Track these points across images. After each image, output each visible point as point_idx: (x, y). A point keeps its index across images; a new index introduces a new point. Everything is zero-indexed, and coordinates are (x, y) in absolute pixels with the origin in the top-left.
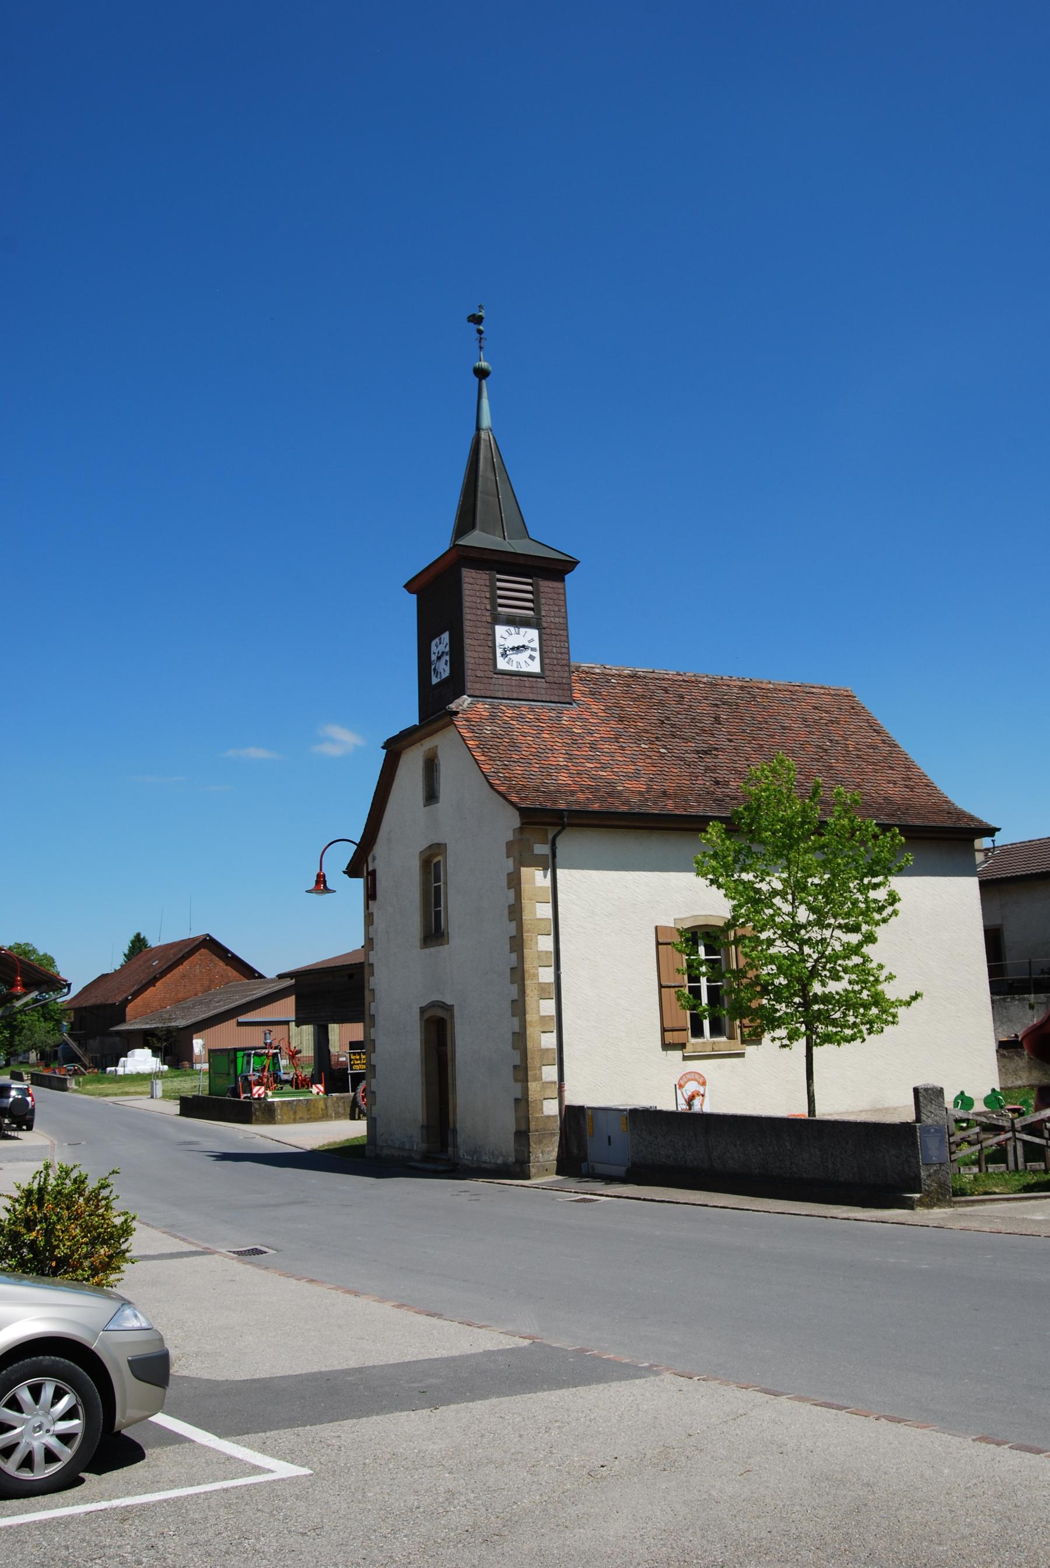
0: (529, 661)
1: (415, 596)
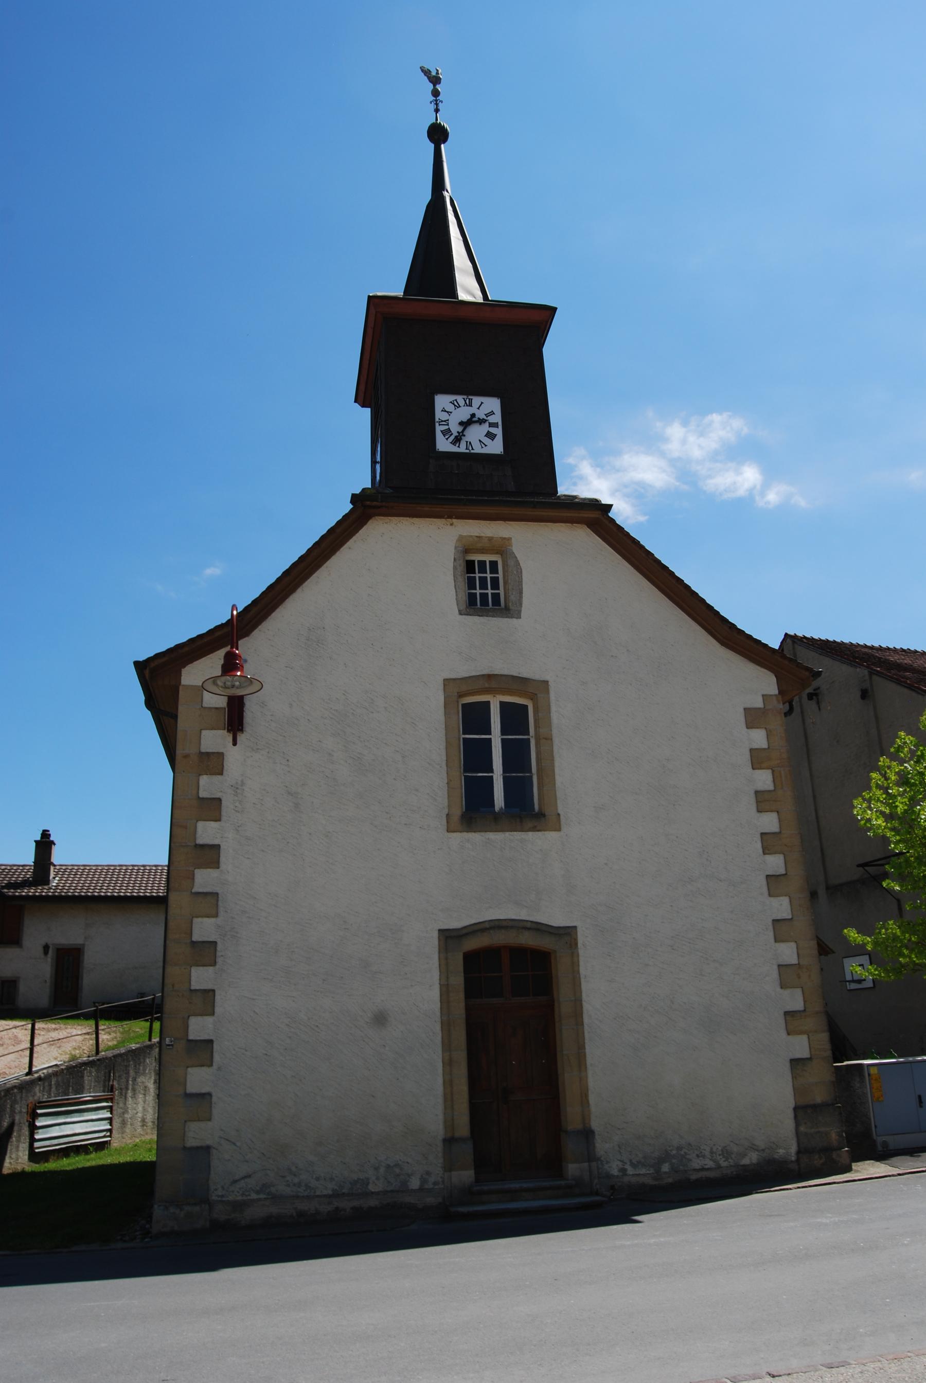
0: (487, 441)
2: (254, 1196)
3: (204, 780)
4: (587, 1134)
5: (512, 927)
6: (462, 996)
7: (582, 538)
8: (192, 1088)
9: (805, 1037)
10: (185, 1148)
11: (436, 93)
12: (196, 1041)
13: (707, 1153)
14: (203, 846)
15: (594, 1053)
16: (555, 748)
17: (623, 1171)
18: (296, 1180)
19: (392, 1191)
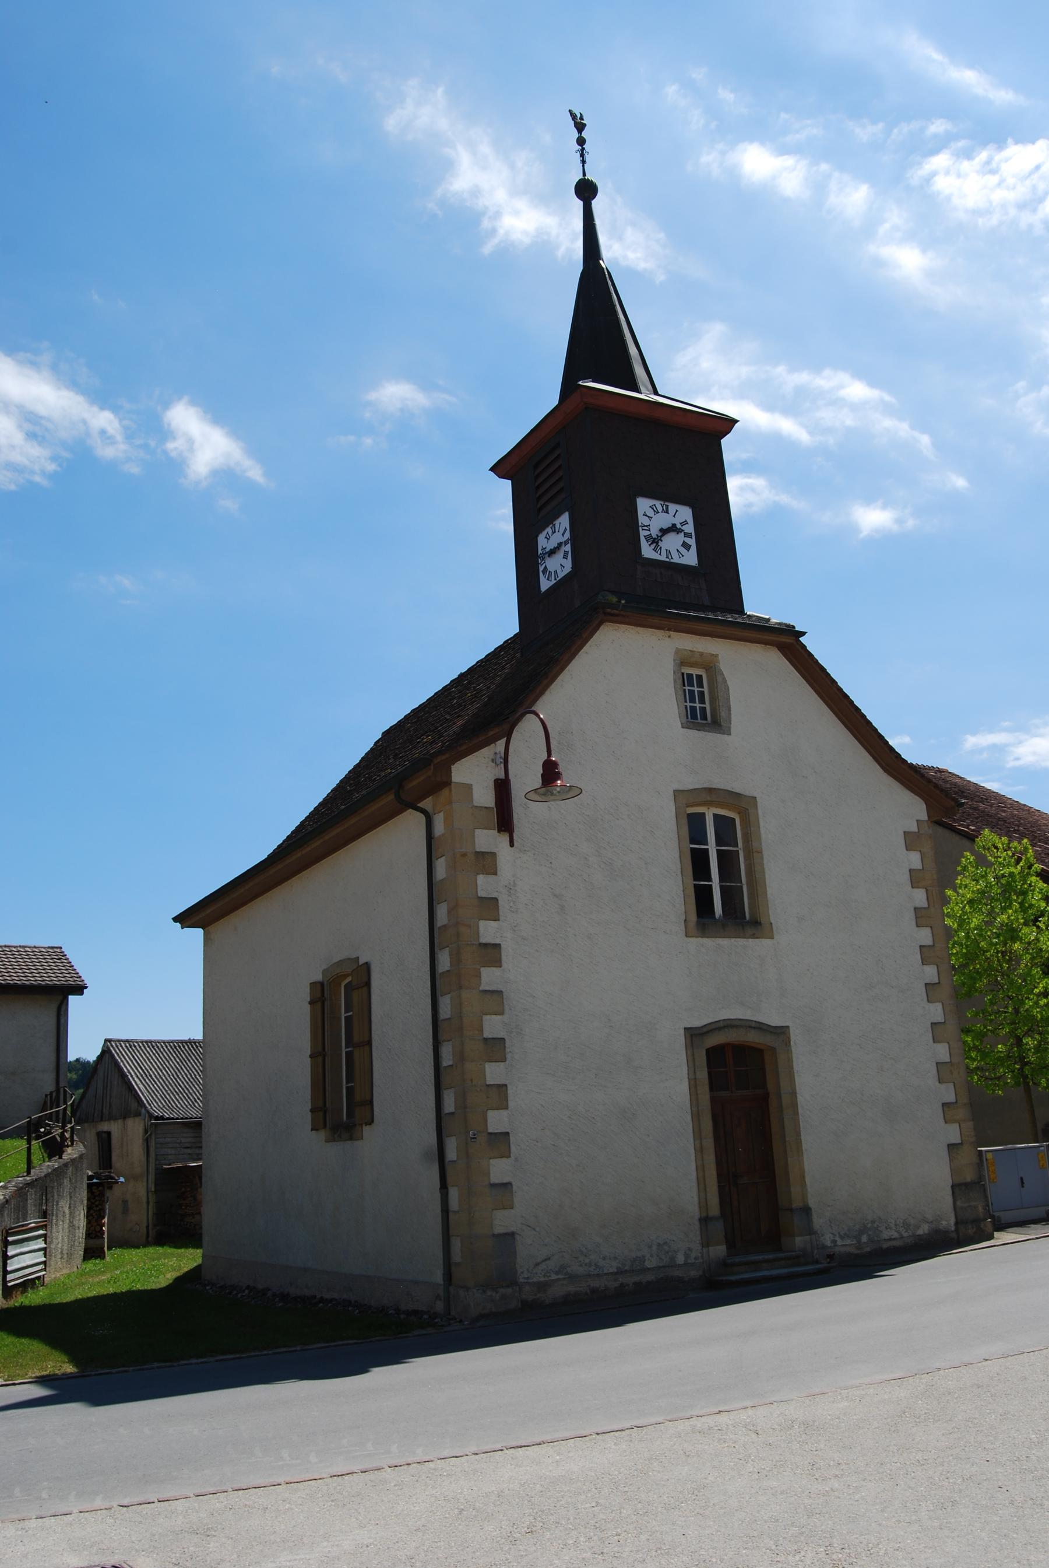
0: (683, 550)
1: (508, 483)
2: (554, 1277)
3: (481, 879)
4: (807, 1210)
5: (741, 1026)
6: (707, 1088)
7: (773, 659)
8: (495, 1179)
9: (957, 1125)
10: (494, 1235)
11: (581, 142)
12: (495, 1134)
13: (892, 1225)
14: (486, 945)
15: (808, 1140)
16: (765, 861)
17: (834, 1242)
18: (587, 1261)
19: (664, 1267)
